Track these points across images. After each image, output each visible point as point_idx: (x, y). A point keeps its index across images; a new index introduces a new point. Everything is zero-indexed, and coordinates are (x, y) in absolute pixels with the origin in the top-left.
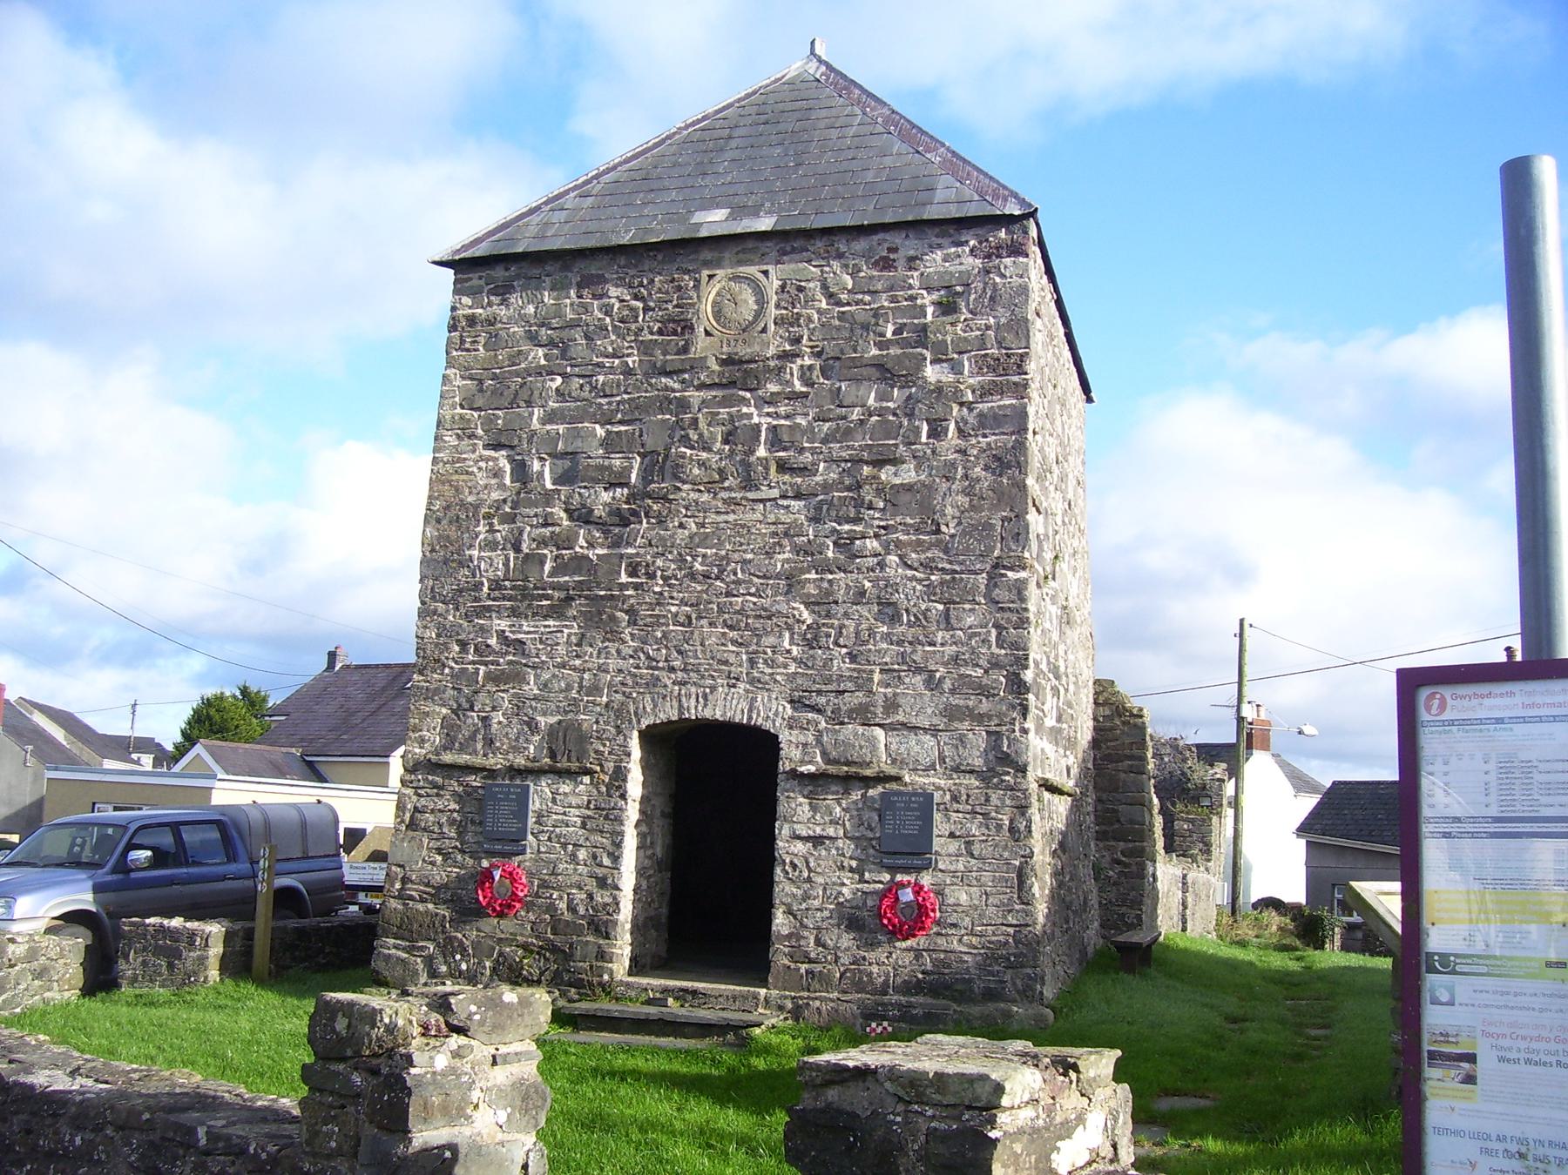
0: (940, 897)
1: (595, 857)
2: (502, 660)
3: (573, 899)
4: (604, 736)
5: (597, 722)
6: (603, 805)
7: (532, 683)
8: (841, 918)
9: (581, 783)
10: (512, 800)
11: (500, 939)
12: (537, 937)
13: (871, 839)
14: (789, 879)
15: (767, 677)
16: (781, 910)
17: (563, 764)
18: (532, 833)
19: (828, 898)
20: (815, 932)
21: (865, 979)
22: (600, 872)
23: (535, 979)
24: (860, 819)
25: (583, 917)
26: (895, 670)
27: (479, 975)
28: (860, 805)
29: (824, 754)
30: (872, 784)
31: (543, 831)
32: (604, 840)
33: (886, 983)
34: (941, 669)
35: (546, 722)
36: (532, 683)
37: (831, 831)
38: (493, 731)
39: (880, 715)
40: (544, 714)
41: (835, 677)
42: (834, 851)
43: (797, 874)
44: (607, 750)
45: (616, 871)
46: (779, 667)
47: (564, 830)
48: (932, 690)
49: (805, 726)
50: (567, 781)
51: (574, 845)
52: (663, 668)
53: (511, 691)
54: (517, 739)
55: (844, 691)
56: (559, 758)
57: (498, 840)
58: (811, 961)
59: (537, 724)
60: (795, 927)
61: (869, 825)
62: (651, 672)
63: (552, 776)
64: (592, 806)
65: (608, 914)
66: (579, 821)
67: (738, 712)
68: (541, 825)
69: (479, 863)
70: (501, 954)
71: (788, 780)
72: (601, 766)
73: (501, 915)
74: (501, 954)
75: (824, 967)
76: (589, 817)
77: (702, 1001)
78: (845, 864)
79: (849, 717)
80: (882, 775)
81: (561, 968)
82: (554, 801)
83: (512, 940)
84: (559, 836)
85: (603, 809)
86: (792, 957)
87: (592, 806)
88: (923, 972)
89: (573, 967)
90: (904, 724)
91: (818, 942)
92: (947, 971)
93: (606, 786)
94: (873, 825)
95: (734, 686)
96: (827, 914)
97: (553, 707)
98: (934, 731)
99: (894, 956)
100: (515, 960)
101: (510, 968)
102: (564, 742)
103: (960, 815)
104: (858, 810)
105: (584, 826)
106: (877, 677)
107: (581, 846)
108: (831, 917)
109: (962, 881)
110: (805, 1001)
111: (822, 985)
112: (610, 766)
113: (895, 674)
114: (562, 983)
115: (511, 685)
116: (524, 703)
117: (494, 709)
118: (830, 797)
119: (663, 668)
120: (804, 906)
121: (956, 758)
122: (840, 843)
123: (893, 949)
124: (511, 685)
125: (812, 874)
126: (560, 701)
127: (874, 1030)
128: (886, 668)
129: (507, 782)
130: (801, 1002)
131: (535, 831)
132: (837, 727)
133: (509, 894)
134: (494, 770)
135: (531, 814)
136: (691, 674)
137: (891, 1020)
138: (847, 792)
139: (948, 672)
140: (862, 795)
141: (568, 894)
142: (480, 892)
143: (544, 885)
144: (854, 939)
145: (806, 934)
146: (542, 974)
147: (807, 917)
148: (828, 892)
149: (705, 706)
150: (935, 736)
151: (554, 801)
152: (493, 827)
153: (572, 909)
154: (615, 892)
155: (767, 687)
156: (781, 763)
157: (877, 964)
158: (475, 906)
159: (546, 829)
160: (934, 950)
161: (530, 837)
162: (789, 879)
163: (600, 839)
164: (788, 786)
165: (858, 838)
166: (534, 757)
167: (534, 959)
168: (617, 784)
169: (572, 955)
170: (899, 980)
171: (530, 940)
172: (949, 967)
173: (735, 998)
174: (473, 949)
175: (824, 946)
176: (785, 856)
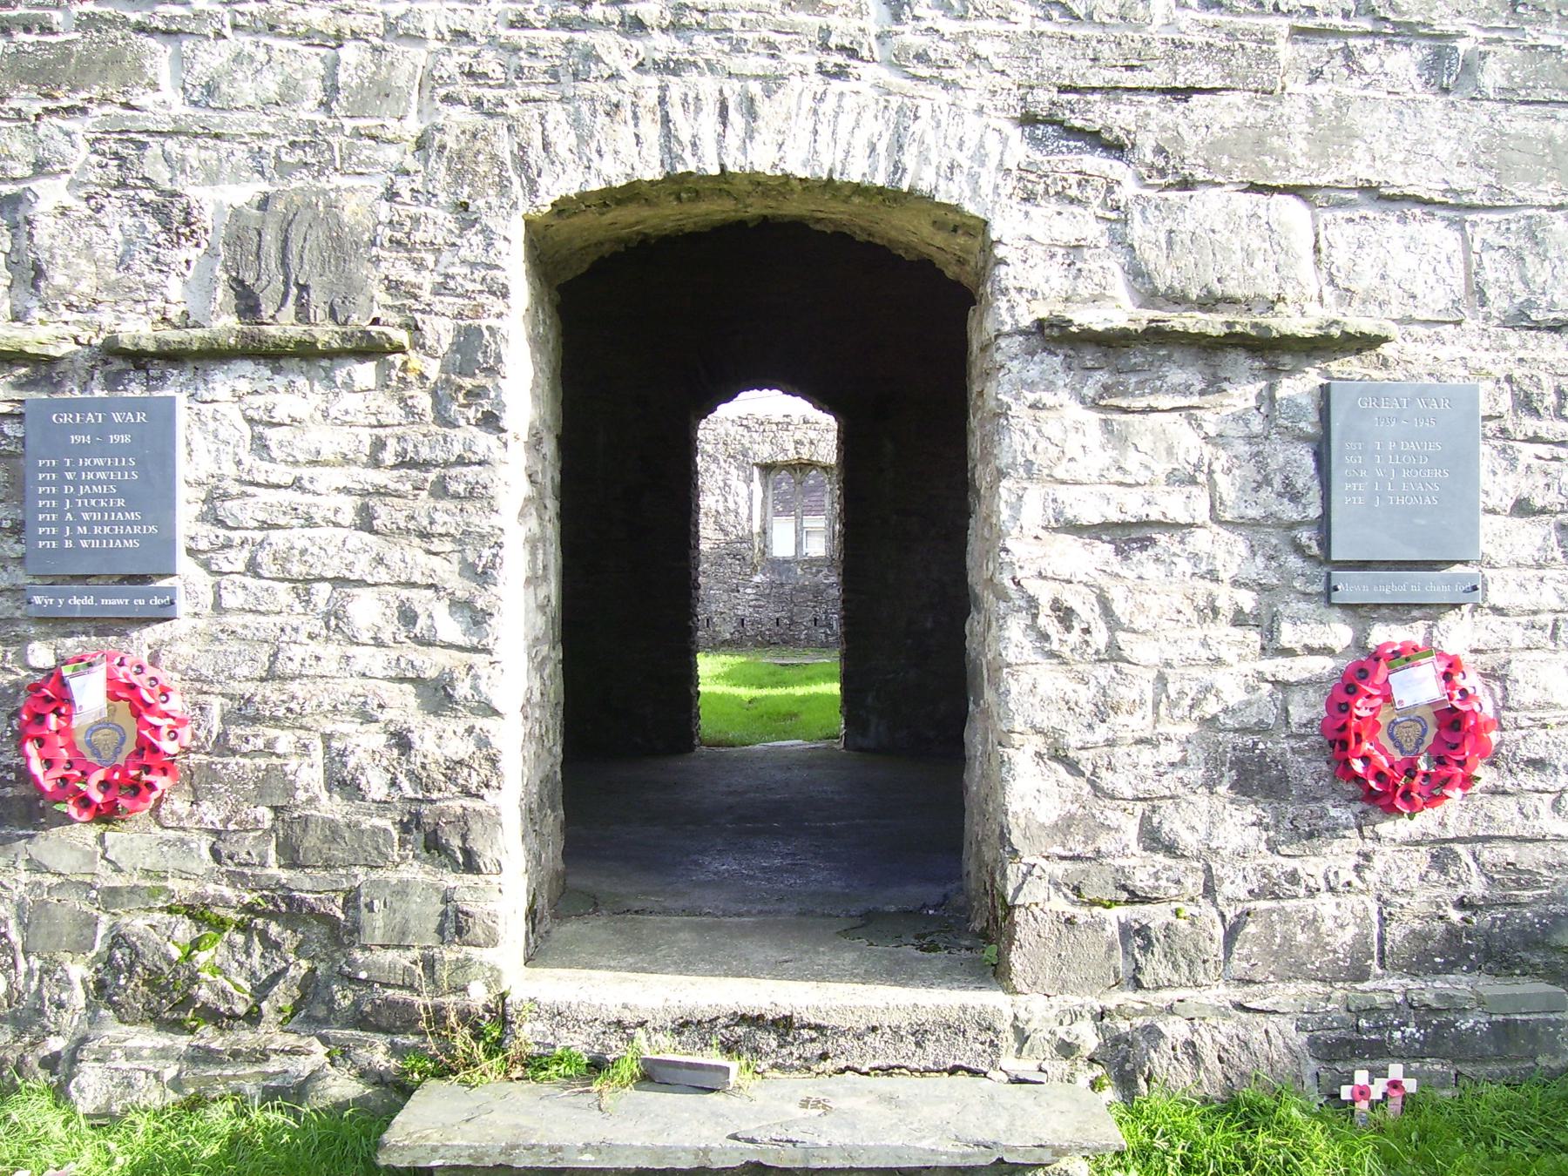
0: (1497, 686)
1: (408, 617)
2: (57, 17)
3: (342, 754)
4: (418, 236)
5: (391, 195)
6: (425, 453)
7: (165, 80)
8: (1214, 762)
9: (349, 386)
10: (119, 451)
11: (114, 891)
12: (236, 879)
13: (1293, 525)
14: (1052, 655)
15: (950, 47)
16: (1030, 750)
17: (283, 326)
18: (191, 552)
19: (1174, 705)
20: (1140, 807)
21: (1301, 938)
22: (432, 663)
23: (241, 1009)
24: (1262, 466)
25: (384, 805)
26: (1335, 33)
27: (50, 1010)
28: (1257, 425)
29: (1137, 273)
30: (1287, 361)
31: (228, 545)
32: (436, 562)
33: (1360, 949)
34: (1472, 31)
35: (219, 205)
36: (165, 80)
37: (1174, 505)
38: (42, 236)
39: (1302, 161)
40: (213, 178)
41: (1158, 49)
42: (1184, 566)
43: (1075, 636)
44: (427, 280)
45: (479, 659)
46: (981, 15)
47: (299, 537)
48: (1446, 91)
49: (1074, 192)
50: (301, 382)
51: (339, 582)
52: (606, 24)
53: (95, 110)
54: (123, 263)
55: (1189, 91)
56: (267, 310)
57: (76, 578)
58: (1135, 898)
59: (187, 212)
60: (1077, 798)
61: (1288, 484)
62: (565, 35)
63: (247, 367)
64: (388, 457)
65: (466, 792)
66: (349, 505)
67: (860, 150)
68: (221, 523)
69: (22, 658)
70: (118, 939)
71: (1032, 354)
72: (414, 328)
73: (106, 815)
74: (118, 939)
75: (1177, 913)
76: (381, 492)
77: (817, 1048)
78: (1223, 603)
79: (1208, 167)
80: (1335, 332)
81: (321, 969)
82: (260, 446)
83: (153, 893)
84: (281, 559)
85: (426, 465)
86: (1077, 890)
87: (388, 457)
88: (1461, 904)
89: (367, 967)
90: (1371, 191)
91: (1153, 839)
92: (1526, 895)
93: (434, 393)
94: (1299, 485)
95: (841, 73)
96: (1171, 752)
97: (241, 154)
98: (1456, 208)
99: (1378, 863)
100: (166, 957)
101: (153, 981)
102: (284, 263)
103: (1542, 450)
104: (1250, 439)
105: (366, 521)
106: (1285, 51)
107: (361, 583)
108: (1184, 762)
109: (1554, 636)
110: (1139, 1022)
111: (1176, 967)
112: (440, 330)
113: (1333, 44)
114: (332, 1016)
115: (96, 92)
116: (143, 146)
117: (40, 168)
118: (1164, 401)
119: (606, 24)
120: (1101, 732)
121: (1518, 286)
122: (1200, 540)
123: (1369, 845)
124: (96, 92)
125: (1121, 637)
126: (264, 136)
127: (1364, 1092)
128: (1310, 23)
129: (99, 393)
130: (1124, 1026)
131: (203, 545)
132: (1173, 195)
133: (130, 746)
134: (52, 361)
135: (183, 493)
136: (699, 39)
137: (1407, 1053)
138: (1214, 385)
139: (1488, 42)
140: (1259, 396)
141: (327, 738)
142: (31, 748)
143: (244, 712)
144: (1258, 823)
145: (1114, 818)
146: (262, 991)
147: (1110, 767)
148: (1172, 690)
149: (750, 134)
150: (1460, 225)
151: (260, 446)
152: (59, 538)
153: (345, 784)
154: (480, 722)
155: (947, 74)
156: (1003, 304)
157: (1332, 889)
158: (22, 791)
159: (236, 536)
160: (1488, 839)
161: (184, 564)
162: (1052, 655)
163: (422, 558)
164: (1033, 372)
165: (1255, 524)
166: (186, 314)
167: (231, 945)
168: (468, 383)
169: (356, 929)
170: (1396, 933)
171: (211, 889)
172: (1533, 883)
173: (920, 1035)
174: (24, 926)
175: (1171, 849)
176: (1033, 587)
